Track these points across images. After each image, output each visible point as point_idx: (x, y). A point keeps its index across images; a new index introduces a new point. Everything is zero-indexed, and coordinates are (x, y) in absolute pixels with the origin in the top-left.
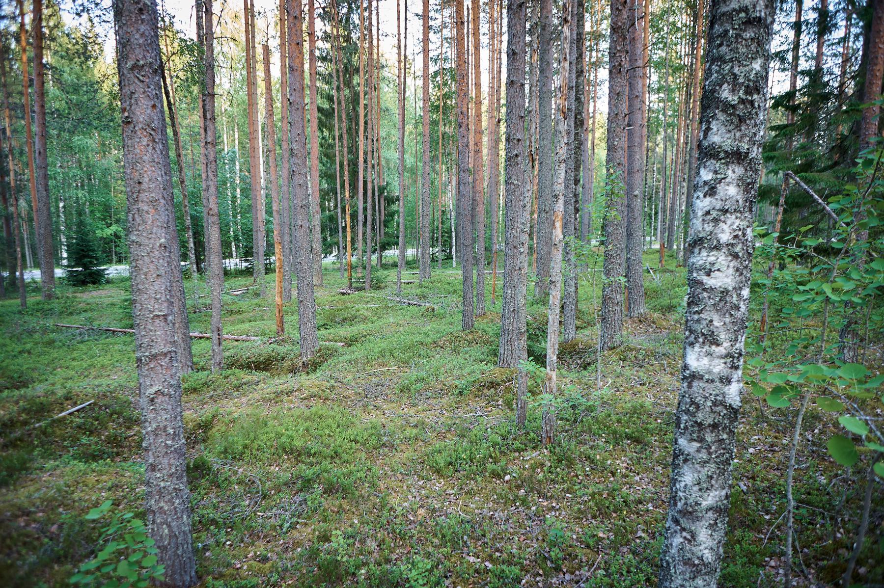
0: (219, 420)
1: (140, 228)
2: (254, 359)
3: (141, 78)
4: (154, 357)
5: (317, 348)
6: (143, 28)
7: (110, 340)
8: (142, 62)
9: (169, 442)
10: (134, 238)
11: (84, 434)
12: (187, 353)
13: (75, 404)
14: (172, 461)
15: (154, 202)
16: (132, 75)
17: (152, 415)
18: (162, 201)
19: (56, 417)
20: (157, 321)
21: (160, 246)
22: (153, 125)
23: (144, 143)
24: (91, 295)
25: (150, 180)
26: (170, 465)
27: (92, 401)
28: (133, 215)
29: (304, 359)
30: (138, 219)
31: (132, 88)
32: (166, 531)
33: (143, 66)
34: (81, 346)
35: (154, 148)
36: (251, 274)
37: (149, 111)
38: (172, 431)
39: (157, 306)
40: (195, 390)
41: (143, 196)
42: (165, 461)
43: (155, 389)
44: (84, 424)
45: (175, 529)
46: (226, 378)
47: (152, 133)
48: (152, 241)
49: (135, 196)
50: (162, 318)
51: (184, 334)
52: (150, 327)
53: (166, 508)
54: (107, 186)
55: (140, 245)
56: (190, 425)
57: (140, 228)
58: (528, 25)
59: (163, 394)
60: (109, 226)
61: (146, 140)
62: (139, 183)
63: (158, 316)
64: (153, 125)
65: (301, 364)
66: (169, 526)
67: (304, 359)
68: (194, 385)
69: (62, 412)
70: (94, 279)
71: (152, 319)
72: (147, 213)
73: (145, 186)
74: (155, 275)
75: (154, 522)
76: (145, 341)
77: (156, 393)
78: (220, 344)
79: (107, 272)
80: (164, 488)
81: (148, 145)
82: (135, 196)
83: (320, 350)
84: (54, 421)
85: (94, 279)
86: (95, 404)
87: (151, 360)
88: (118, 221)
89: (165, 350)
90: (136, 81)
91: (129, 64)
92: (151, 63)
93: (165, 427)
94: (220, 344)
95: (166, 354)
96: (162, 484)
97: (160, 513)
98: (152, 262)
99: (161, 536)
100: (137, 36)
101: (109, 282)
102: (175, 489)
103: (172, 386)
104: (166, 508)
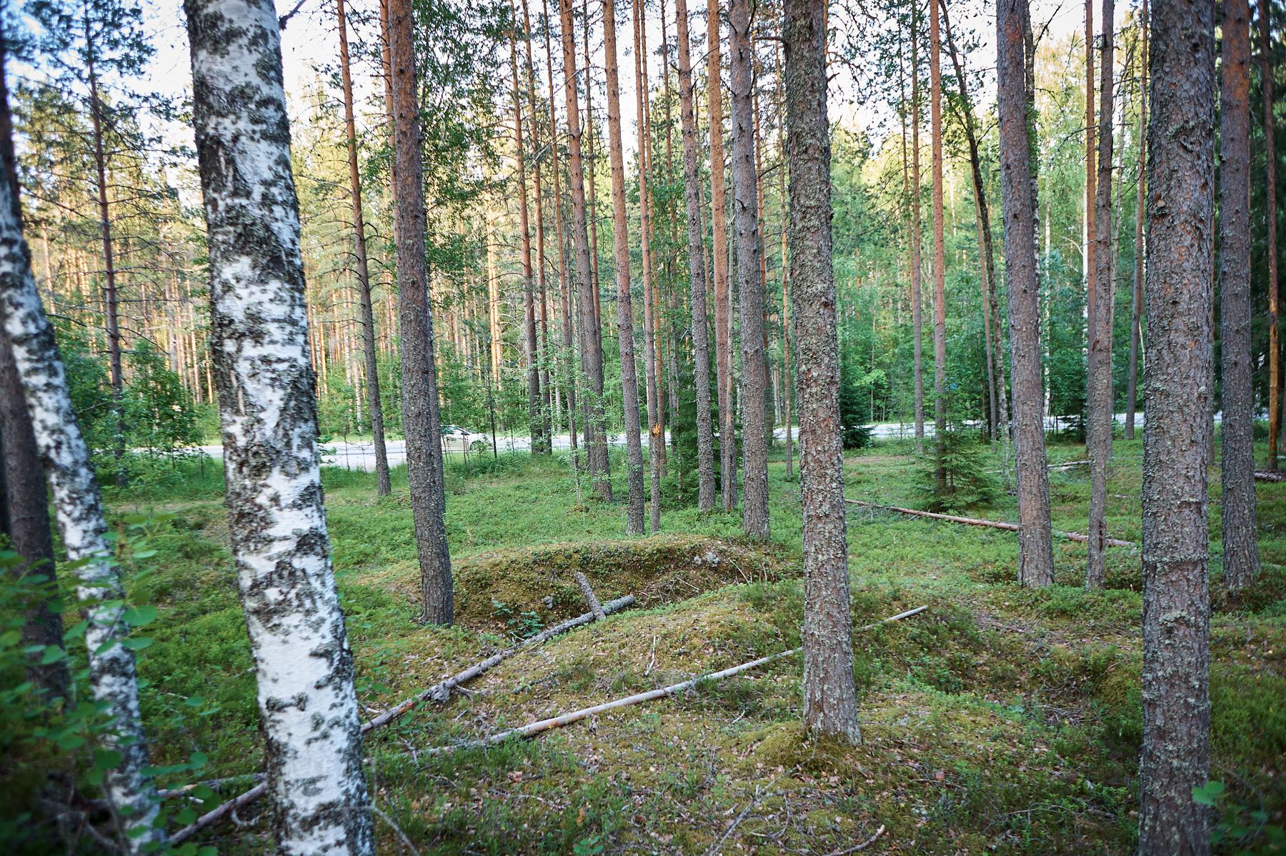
0: (1118, 667)
1: (1170, 370)
2: (1131, 576)
3: (1189, 147)
4: (1177, 565)
5: (1258, 572)
6: (1195, 72)
7: (900, 524)
8: (1192, 123)
9: (1192, 700)
10: (1158, 385)
11: (922, 649)
12: (1047, 556)
13: (905, 607)
14: (1194, 730)
15: (1193, 330)
16: (1175, 145)
17: (1167, 654)
18: (1206, 328)
19: (886, 620)
20: (1187, 511)
21: (1200, 396)
22: (1202, 214)
23: (1187, 243)
24: (855, 463)
25: (1190, 298)
26: (1191, 736)
27: (925, 607)
28: (1159, 351)
29: (1231, 587)
30: (1167, 357)
31: (1173, 164)
32: (1177, 837)
33: (1193, 128)
34: (868, 528)
35: (1200, 249)
36: (1082, 440)
37: (1197, 195)
38: (1197, 684)
39: (1187, 489)
40: (1063, 613)
41: (1179, 322)
42: (1183, 728)
43: (1176, 614)
44: (920, 636)
45: (1191, 838)
46: (1113, 601)
47: (1200, 226)
48: (1188, 389)
49: (1165, 323)
50: (1193, 507)
51: (1044, 527)
52: (1173, 518)
53: (1180, 802)
54: (869, 320)
55: (1168, 396)
56: (1069, 666)
57: (1170, 370)
58: (1256, 17)
59: (1188, 624)
60: (869, 371)
61: (1189, 238)
62: (1175, 303)
63: (1189, 504)
64: (1202, 214)
65: (1224, 595)
66: (1182, 831)
67: (1231, 587)
68: (1063, 605)
69: (891, 614)
70: (856, 441)
71: (1179, 507)
72: (1183, 347)
73: (1182, 307)
74: (1187, 441)
75: (1156, 817)
76: (1166, 539)
77: (1176, 620)
78: (1101, 548)
79: (872, 432)
80: (1178, 769)
81: (1192, 245)
82: (1165, 323)
83: (1263, 575)
84: (885, 625)
85: (856, 441)
86: (928, 610)
87: (1172, 569)
88: (880, 365)
89: (1195, 557)
90: (1181, 152)
91: (1171, 129)
92: (1204, 122)
93: (1188, 675)
94: (1101, 548)
95: (1195, 564)
96: (1175, 763)
97: (1167, 806)
98: (1186, 420)
99: (1168, 843)
100: (1187, 86)
101: (876, 445)
102: (1194, 774)
103: (1201, 613)
104: (1180, 802)
